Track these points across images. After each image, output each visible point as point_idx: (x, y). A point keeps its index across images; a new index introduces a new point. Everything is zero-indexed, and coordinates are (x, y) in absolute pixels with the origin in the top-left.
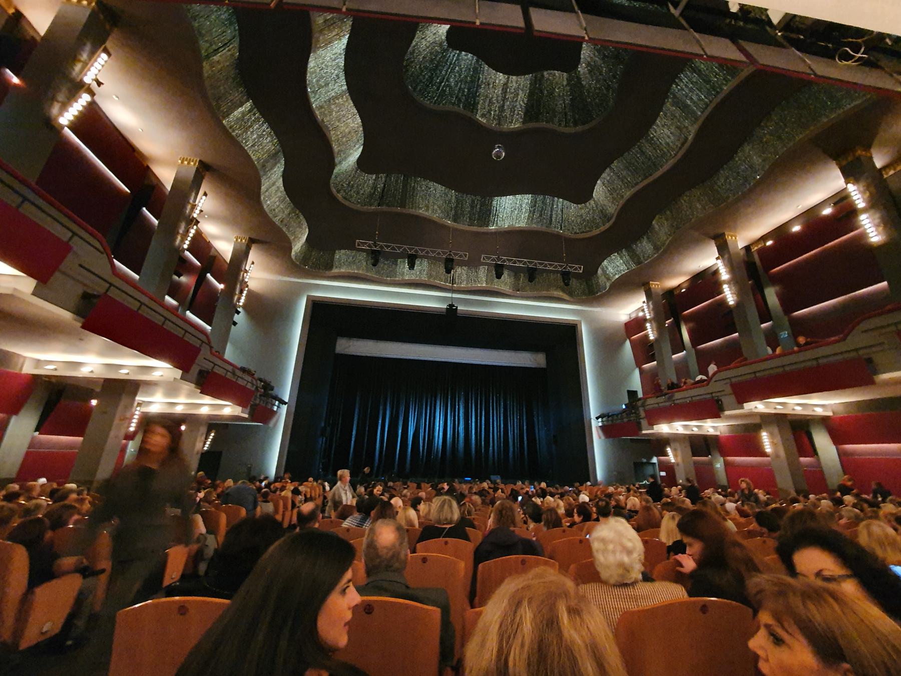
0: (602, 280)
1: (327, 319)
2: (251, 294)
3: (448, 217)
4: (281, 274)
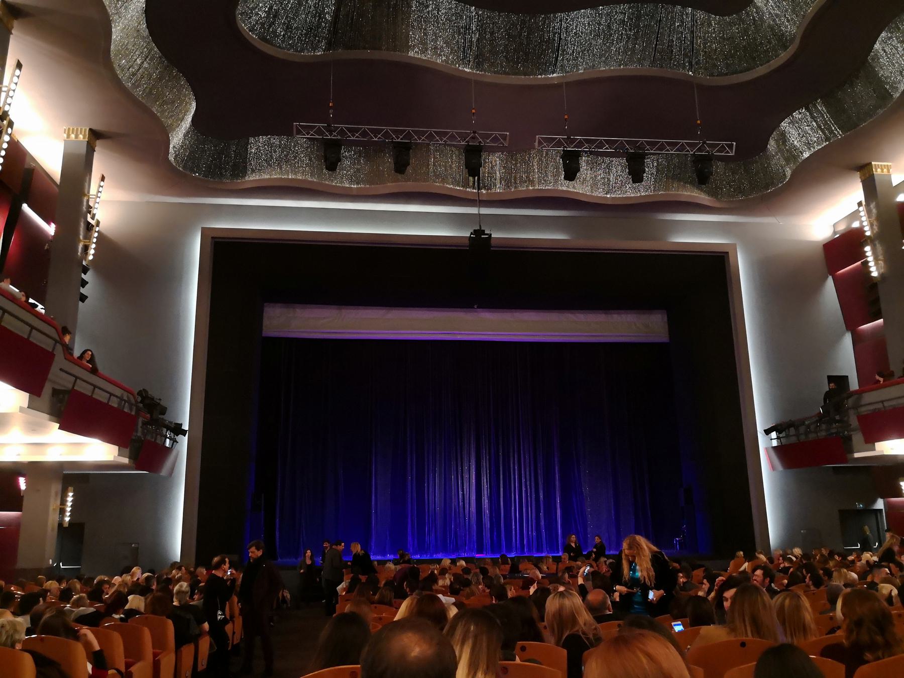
0: (777, 161)
1: (229, 258)
2: (103, 240)
3: (464, 60)
4: (150, 191)
